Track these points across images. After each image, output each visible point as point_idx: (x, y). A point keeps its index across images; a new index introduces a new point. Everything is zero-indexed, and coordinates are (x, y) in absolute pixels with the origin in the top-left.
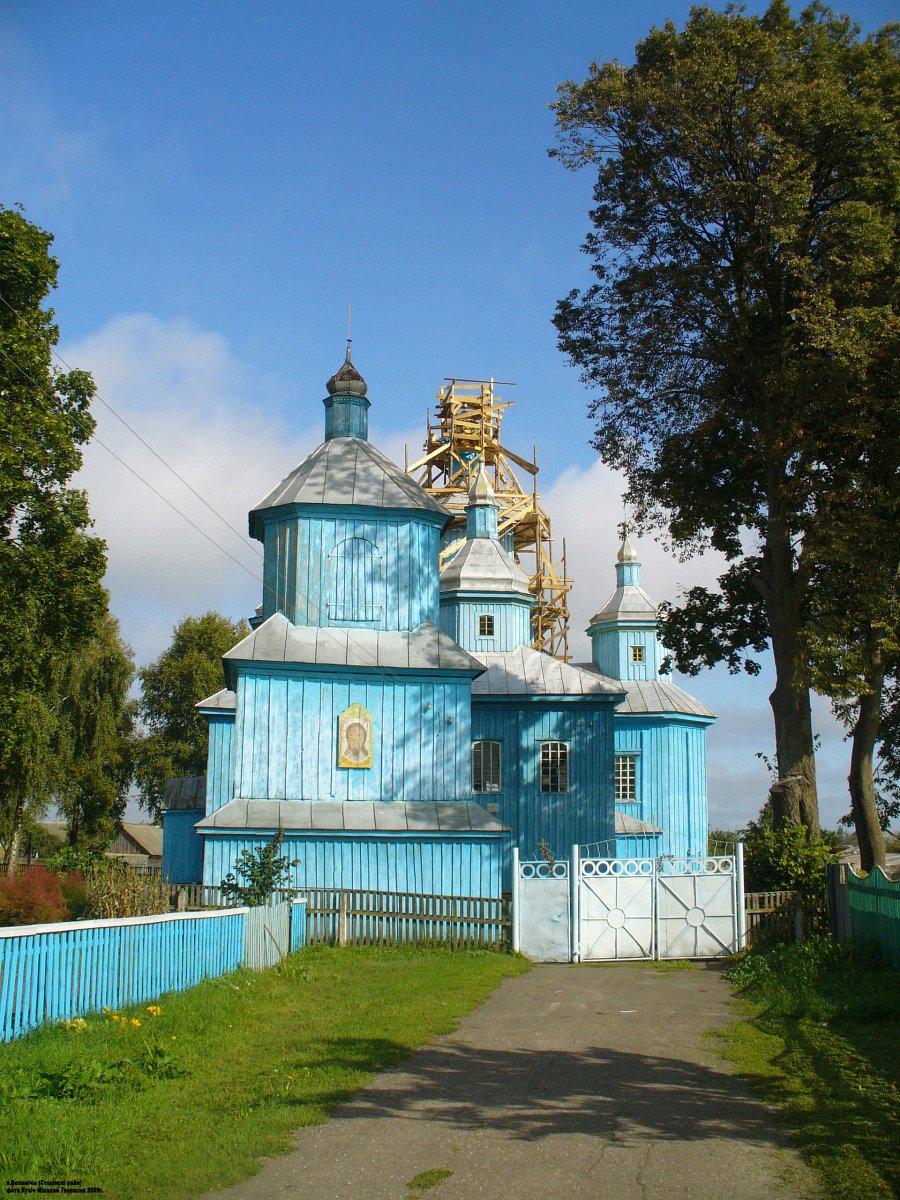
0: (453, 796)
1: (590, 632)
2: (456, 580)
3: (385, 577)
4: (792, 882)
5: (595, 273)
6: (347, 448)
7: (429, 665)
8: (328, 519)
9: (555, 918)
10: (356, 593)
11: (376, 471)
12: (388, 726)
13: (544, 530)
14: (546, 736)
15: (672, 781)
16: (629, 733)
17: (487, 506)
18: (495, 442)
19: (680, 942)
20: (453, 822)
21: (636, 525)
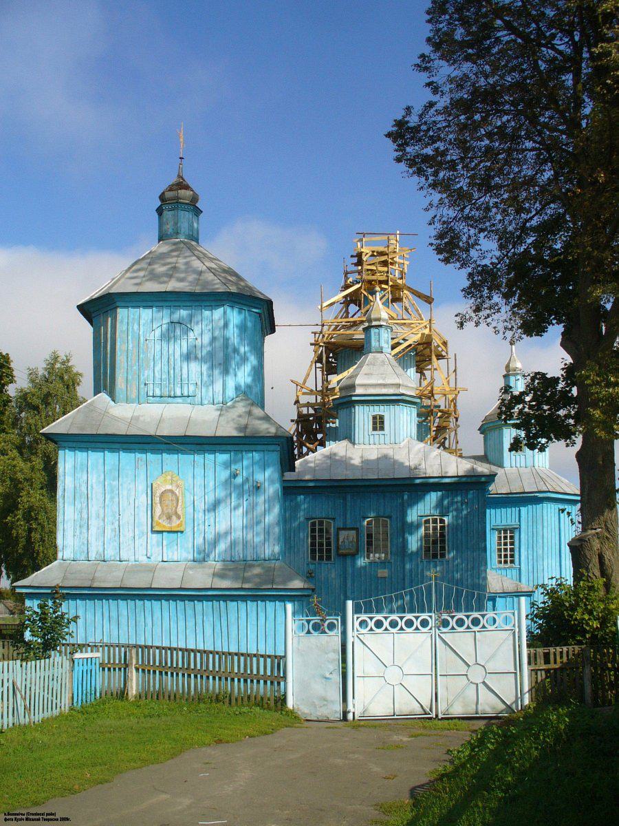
0: (263, 556)
1: (482, 430)
2: (352, 387)
3: (199, 356)
4: (588, 636)
5: (428, 90)
6: (174, 247)
7: (235, 434)
8: (145, 307)
9: (328, 675)
10: (172, 372)
11: (196, 264)
12: (199, 491)
13: (443, 350)
14: (427, 512)
15: (546, 549)
16: (509, 510)
17: (381, 326)
18: (400, 282)
19: (461, 699)
20: (257, 580)
21: (473, 315)
